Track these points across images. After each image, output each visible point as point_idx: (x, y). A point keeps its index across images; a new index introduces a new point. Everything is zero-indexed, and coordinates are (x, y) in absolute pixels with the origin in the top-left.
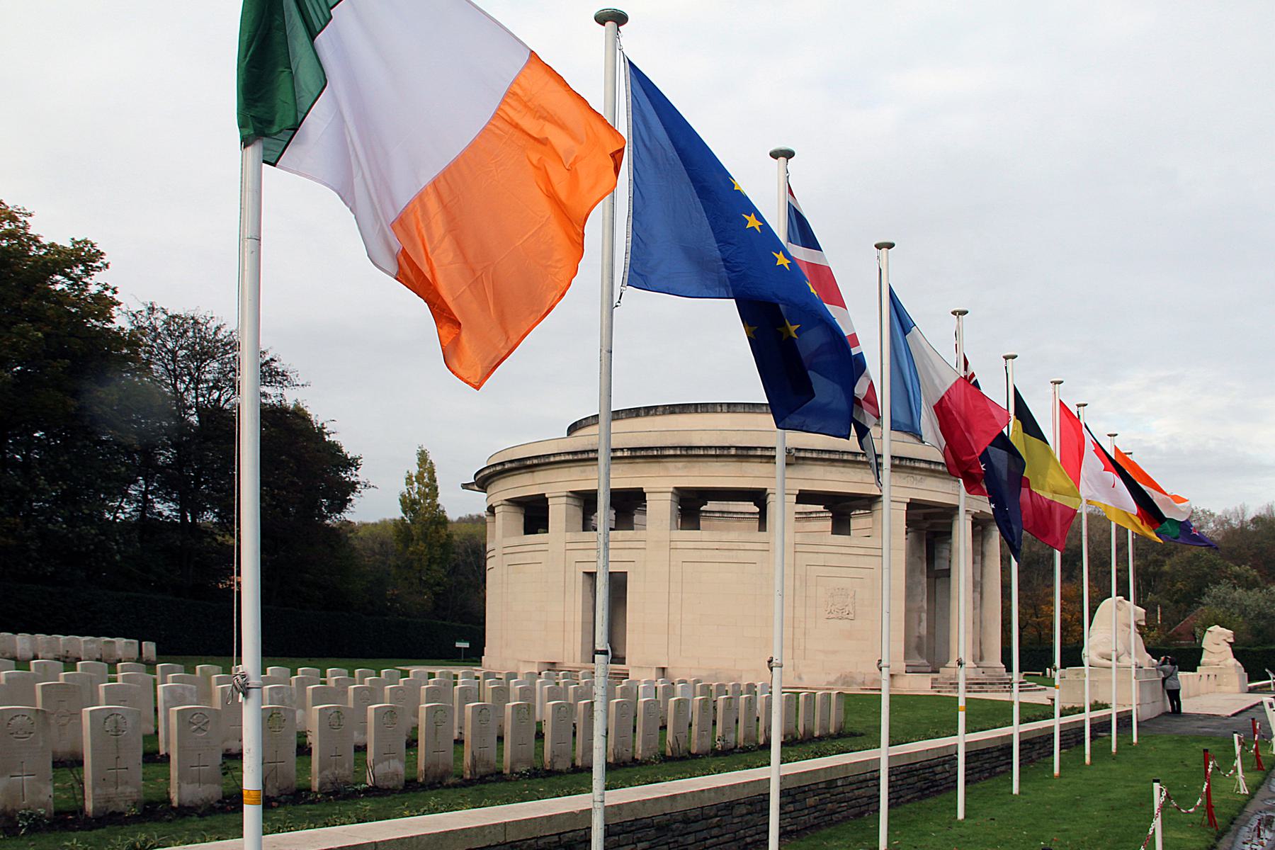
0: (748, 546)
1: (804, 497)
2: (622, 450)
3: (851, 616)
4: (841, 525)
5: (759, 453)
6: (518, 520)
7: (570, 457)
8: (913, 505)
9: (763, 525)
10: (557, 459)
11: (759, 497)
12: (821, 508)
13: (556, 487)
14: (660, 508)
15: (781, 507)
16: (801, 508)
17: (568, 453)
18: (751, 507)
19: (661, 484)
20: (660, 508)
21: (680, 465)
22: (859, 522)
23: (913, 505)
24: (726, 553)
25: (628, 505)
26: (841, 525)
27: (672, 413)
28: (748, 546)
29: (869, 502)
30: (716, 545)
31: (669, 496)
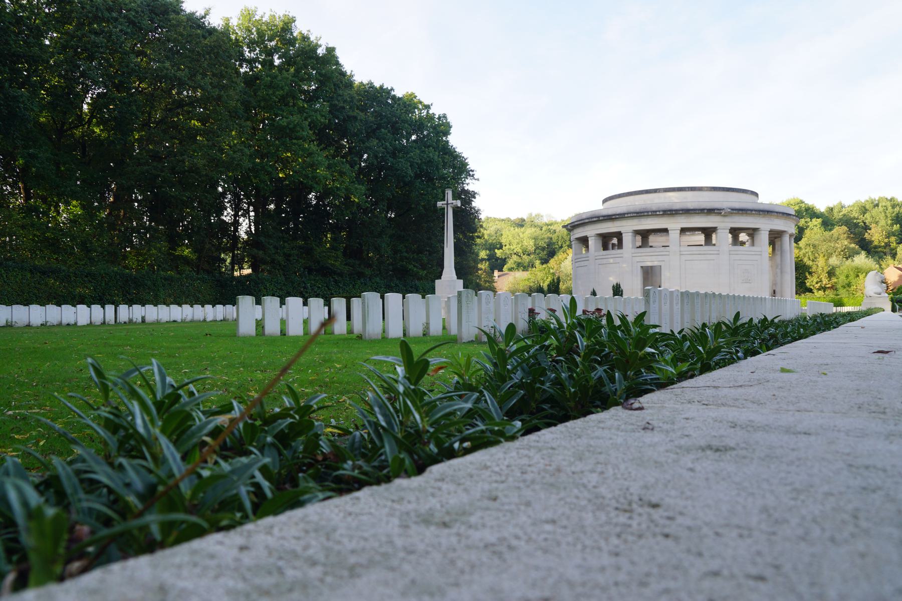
15: (627, 239)
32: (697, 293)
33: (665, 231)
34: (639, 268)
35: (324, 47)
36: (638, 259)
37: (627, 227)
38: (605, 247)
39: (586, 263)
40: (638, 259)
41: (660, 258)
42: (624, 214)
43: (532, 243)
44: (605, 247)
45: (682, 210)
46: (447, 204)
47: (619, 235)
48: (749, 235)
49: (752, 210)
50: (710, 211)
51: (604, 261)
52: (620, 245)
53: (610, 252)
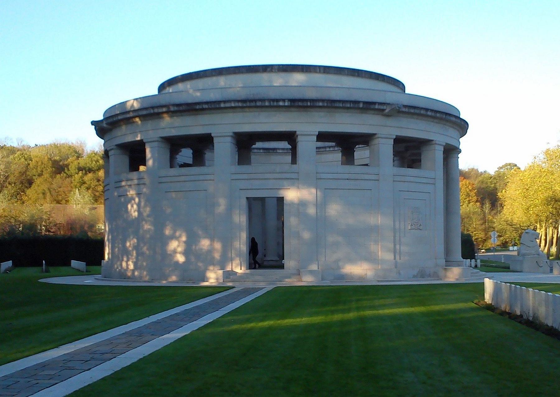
0: (183, 178)
1: (322, 137)
2: (284, 100)
3: (421, 227)
4: (348, 156)
5: (377, 107)
6: (125, 160)
7: (240, 104)
8: (398, 141)
9: (294, 161)
10: (228, 105)
11: (290, 137)
12: (334, 144)
13: (223, 128)
14: (224, 148)
15: (307, 145)
16: (320, 144)
17: (238, 101)
18: (285, 145)
19: (387, 130)
20: (224, 148)
21: (322, 114)
22: (361, 154)
23: (398, 141)
24: (352, 182)
25: (201, 145)
26: (348, 156)
27: (353, 75)
28: (367, 177)
29: (365, 139)
30: (347, 176)
31: (229, 139)
42: (219, 102)
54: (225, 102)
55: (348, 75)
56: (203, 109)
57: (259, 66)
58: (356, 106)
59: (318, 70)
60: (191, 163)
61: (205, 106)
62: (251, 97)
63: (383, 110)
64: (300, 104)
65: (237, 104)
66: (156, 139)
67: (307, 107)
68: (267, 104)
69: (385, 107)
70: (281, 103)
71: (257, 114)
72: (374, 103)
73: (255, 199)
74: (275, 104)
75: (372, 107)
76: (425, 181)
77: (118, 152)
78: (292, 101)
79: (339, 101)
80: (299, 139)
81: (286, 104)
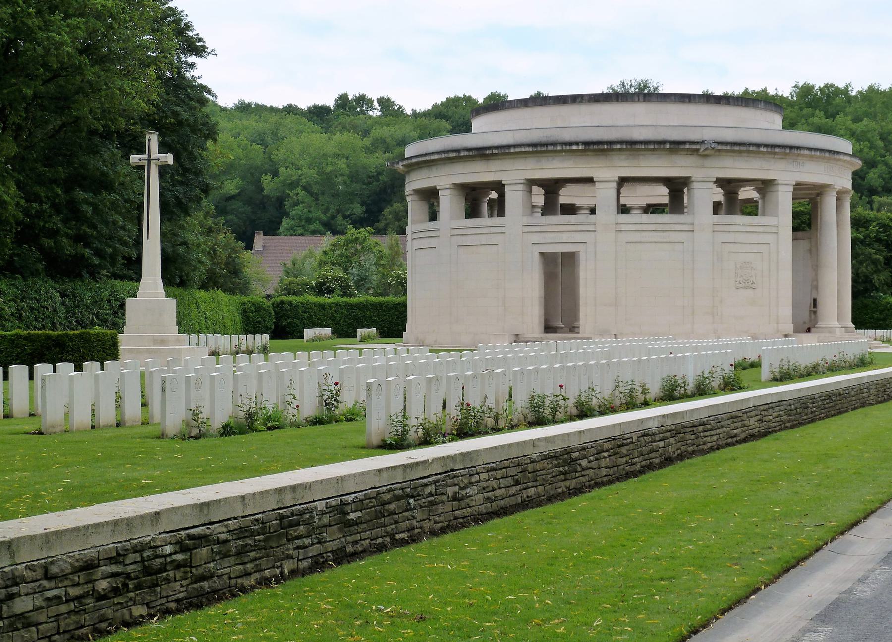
2: (577, 143)
5: (687, 146)
7: (530, 149)
10: (518, 150)
15: (514, 198)
17: (529, 145)
32: (290, 110)
33: (590, 181)
34: (537, 256)
35: (195, 32)
36: (536, 238)
37: (513, 174)
38: (472, 212)
39: (433, 242)
40: (536, 238)
41: (578, 237)
42: (509, 146)
43: (313, 172)
44: (472, 212)
45: (621, 142)
46: (149, 160)
47: (499, 187)
48: (759, 190)
49: (758, 145)
50: (676, 147)
51: (469, 240)
52: (499, 207)
53: (485, 221)
54: (515, 146)
55: (675, 101)
56: (493, 154)
57: (567, 96)
58: (662, 146)
59: (637, 99)
60: (666, 200)
61: (495, 151)
62: (544, 140)
63: (698, 150)
64: (595, 147)
65: (527, 149)
66: (448, 186)
67: (603, 150)
68: (559, 148)
69: (698, 147)
70: (574, 147)
71: (550, 159)
72: (684, 143)
73: (749, 214)
74: (568, 147)
75: (682, 147)
76: (761, 229)
77: (415, 198)
78: (587, 143)
79: (641, 142)
80: (507, 188)
81: (580, 147)
